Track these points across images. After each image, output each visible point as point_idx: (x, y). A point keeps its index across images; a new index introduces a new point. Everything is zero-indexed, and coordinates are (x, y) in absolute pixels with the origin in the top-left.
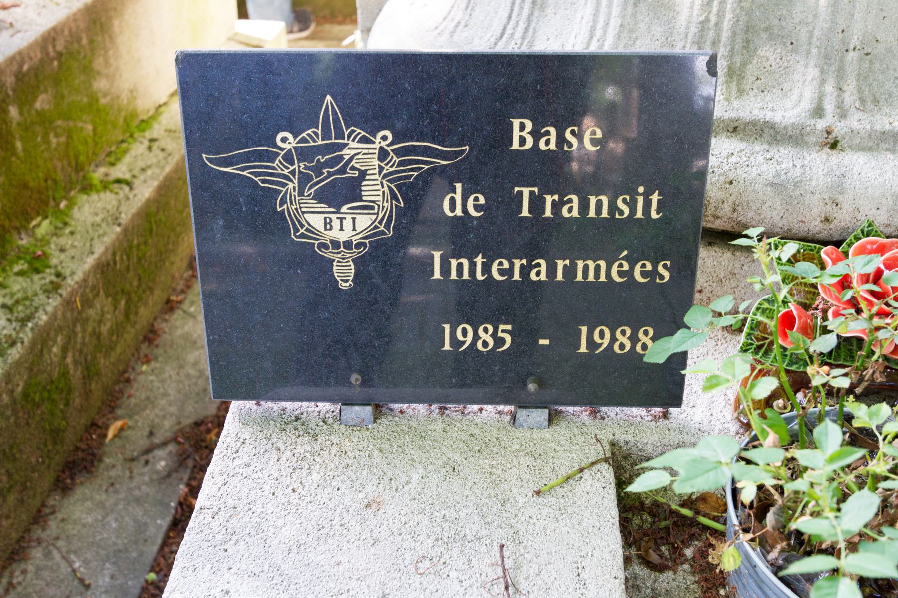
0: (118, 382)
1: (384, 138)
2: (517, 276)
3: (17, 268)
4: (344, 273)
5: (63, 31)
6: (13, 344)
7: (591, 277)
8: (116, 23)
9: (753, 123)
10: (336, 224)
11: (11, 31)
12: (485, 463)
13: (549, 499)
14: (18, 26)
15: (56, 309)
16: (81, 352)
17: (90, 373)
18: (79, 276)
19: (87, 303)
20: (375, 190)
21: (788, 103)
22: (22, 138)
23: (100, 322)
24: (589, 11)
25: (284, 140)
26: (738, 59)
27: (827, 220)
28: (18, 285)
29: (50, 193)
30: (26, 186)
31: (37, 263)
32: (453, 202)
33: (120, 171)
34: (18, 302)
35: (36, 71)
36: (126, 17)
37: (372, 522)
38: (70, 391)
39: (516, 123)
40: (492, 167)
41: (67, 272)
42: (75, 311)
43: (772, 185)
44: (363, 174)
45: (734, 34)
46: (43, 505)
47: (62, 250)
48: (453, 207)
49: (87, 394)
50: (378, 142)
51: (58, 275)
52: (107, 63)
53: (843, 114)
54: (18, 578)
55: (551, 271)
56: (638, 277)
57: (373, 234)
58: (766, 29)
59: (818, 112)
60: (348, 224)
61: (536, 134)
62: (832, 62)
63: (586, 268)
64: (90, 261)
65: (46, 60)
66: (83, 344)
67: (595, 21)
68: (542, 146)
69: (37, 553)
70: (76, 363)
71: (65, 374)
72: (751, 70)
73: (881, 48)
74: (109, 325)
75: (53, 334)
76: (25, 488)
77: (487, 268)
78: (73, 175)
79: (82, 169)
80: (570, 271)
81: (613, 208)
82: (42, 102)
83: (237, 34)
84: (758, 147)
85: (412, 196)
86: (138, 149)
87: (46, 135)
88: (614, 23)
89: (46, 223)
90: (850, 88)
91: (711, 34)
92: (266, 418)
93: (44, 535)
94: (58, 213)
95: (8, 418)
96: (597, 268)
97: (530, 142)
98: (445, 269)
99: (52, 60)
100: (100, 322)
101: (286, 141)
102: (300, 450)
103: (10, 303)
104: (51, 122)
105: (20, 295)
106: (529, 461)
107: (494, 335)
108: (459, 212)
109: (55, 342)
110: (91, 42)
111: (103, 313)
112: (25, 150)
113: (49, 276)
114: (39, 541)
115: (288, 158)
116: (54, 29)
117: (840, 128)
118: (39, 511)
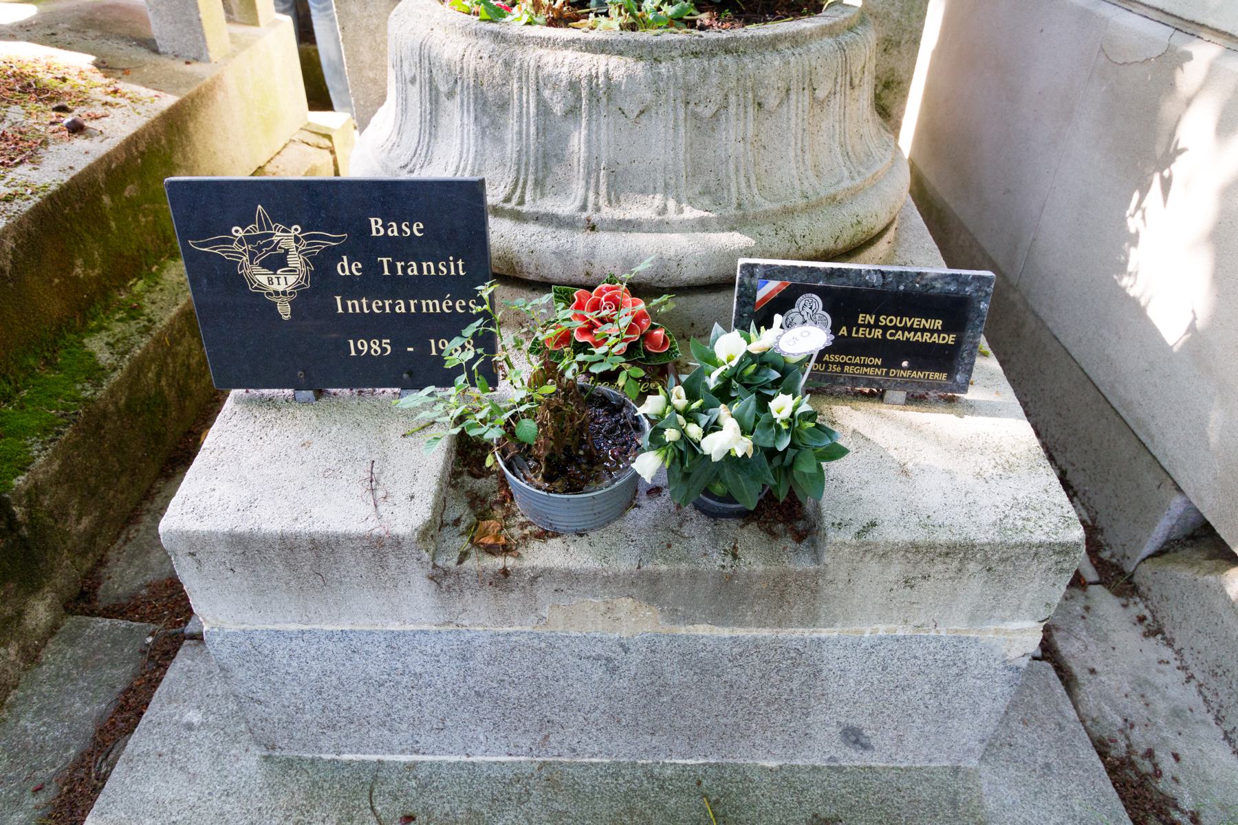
0: (211, 402)
1: (296, 230)
2: (388, 310)
3: (117, 316)
4: (284, 310)
5: (143, 136)
6: (115, 370)
7: (431, 310)
8: (191, 125)
9: (546, 215)
10: (275, 281)
11: (101, 138)
12: (378, 421)
13: (411, 439)
14: (106, 132)
15: (147, 345)
16: (173, 377)
17: (183, 393)
18: (166, 321)
19: (175, 341)
20: (295, 260)
21: (569, 202)
22: (115, 219)
23: (188, 356)
24: (458, 141)
25: (237, 231)
26: (540, 174)
27: (588, 274)
28: (118, 328)
29: (143, 260)
30: (121, 256)
31: (134, 312)
32: (342, 266)
34: (118, 340)
35: (123, 168)
36: (200, 119)
37: (304, 452)
38: (166, 406)
39: (372, 220)
40: (366, 248)
41: (157, 318)
42: (165, 348)
43: (554, 253)
44: (287, 251)
45: (537, 159)
46: (151, 487)
47: (153, 303)
48: (343, 271)
49: (182, 409)
50: (293, 233)
51: (150, 321)
52: (185, 157)
54: (133, 534)
55: (408, 307)
56: (459, 310)
57: (298, 286)
58: (555, 156)
59: (584, 208)
60: (282, 280)
61: (385, 227)
63: (427, 305)
64: (175, 310)
65: (130, 159)
66: (175, 371)
67: (462, 148)
68: (390, 233)
70: (170, 386)
71: (160, 393)
72: (549, 181)
73: (621, 168)
74: (197, 358)
75: (146, 363)
76: (134, 474)
77: (369, 307)
78: (162, 246)
79: (170, 241)
80: (418, 307)
81: (437, 269)
82: (130, 191)
83: (309, 124)
84: (549, 230)
85: (321, 265)
87: (135, 217)
88: (472, 150)
89: (141, 283)
90: (603, 189)
91: (524, 159)
92: (251, 400)
93: (152, 507)
94: (150, 274)
95: (115, 422)
96: (434, 305)
97: (382, 232)
98: (345, 307)
99: (136, 159)
100: (188, 356)
101: (238, 232)
102: (268, 416)
103: (112, 341)
104: (139, 206)
105: (119, 336)
106: (404, 419)
107: (380, 346)
108: (347, 273)
109: (150, 370)
110: (169, 141)
111: (190, 350)
112: (118, 228)
113: (143, 322)
114: (148, 511)
115: (240, 242)
116: (135, 134)
117: (595, 218)
118: (148, 491)
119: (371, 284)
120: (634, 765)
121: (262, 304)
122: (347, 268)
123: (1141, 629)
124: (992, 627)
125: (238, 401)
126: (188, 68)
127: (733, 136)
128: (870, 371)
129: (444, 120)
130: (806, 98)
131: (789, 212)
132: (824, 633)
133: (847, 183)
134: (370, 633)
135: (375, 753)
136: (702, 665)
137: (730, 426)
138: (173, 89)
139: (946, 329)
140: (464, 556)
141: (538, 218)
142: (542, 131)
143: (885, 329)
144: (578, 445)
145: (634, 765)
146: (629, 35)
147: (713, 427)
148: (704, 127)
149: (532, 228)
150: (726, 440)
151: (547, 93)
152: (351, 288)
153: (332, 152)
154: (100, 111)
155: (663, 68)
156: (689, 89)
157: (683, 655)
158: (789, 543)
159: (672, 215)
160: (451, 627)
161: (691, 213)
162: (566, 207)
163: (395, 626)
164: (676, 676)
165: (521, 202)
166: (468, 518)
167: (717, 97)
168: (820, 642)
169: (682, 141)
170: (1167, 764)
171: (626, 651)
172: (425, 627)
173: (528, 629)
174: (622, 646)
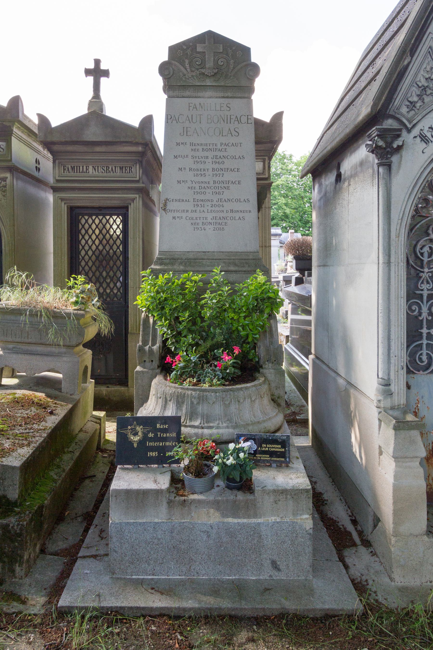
4: (135, 445)
20: (140, 434)
31: (59, 467)
33: (70, 449)
40: (155, 430)
53: (204, 424)
57: (139, 439)
59: (201, 424)
62: (203, 417)
69: (55, 535)
85: (145, 436)
86: (74, 444)
90: (205, 420)
101: (129, 427)
117: (203, 426)
119: (156, 439)
120: (215, 579)
121: (131, 443)
122: (151, 435)
123: (371, 554)
124: (299, 518)
125: (120, 468)
126: (71, 396)
127: (233, 408)
128: (267, 458)
129: (168, 406)
130: (249, 400)
131: (248, 425)
132: (260, 520)
133: (262, 419)
134: (150, 522)
135: (142, 575)
136: (231, 532)
137: (231, 458)
138: (70, 402)
139: (282, 447)
140: (175, 497)
141: (190, 426)
142: (191, 407)
143: (269, 448)
144: (201, 466)
145: (215, 579)
146: (210, 388)
147: (228, 460)
148: (227, 406)
149: (189, 429)
150: (231, 461)
151: (193, 400)
152: (151, 440)
153: (100, 425)
154: (54, 409)
155: (217, 394)
156: (223, 398)
157: (226, 530)
158: (249, 494)
159: (221, 425)
160: (170, 521)
161: (225, 425)
162: (197, 423)
163: (156, 520)
164: (225, 539)
165: (186, 423)
166: (175, 491)
167: (230, 400)
168: (259, 524)
169: (222, 409)
170: (370, 582)
171: (212, 528)
172: (164, 521)
173: (188, 521)
174: (211, 526)
